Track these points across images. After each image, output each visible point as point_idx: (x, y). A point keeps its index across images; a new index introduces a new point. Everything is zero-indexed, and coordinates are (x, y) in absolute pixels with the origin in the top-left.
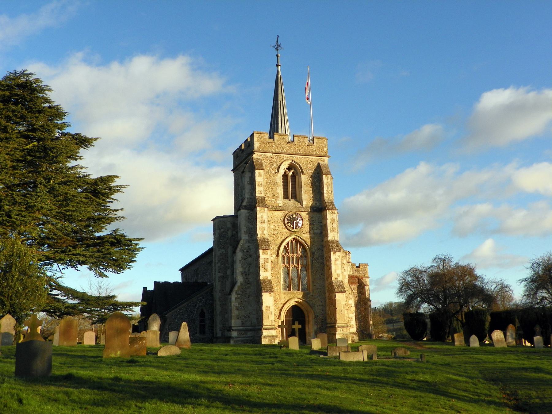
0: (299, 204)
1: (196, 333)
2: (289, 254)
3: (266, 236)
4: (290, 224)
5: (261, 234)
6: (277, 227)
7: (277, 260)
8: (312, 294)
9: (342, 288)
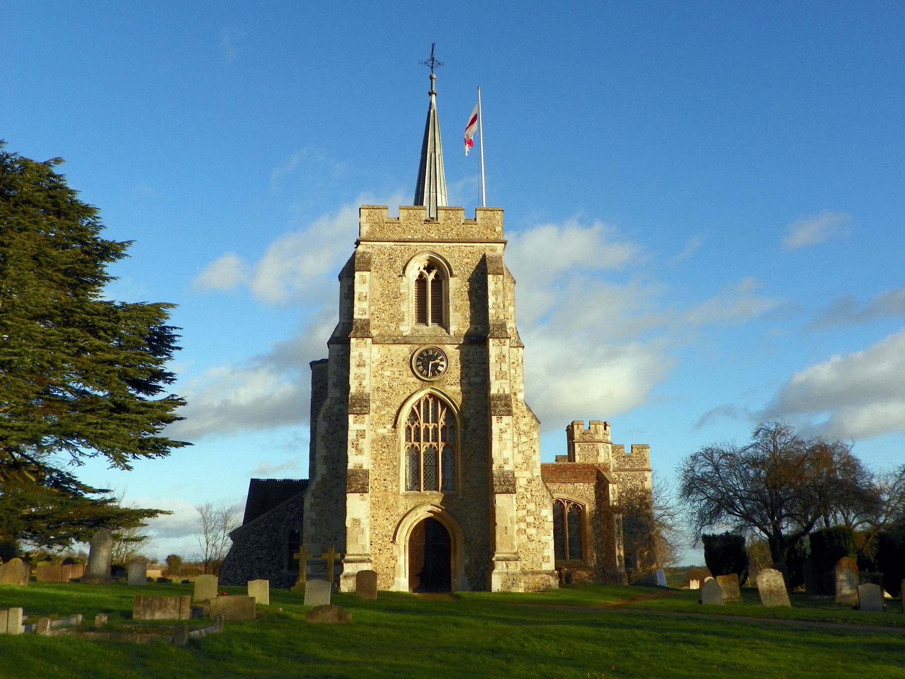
0: (444, 330)
1: (282, 567)
2: (419, 423)
3: (367, 390)
4: (421, 367)
5: (356, 387)
6: (397, 375)
7: (394, 434)
8: (461, 497)
9: (510, 485)
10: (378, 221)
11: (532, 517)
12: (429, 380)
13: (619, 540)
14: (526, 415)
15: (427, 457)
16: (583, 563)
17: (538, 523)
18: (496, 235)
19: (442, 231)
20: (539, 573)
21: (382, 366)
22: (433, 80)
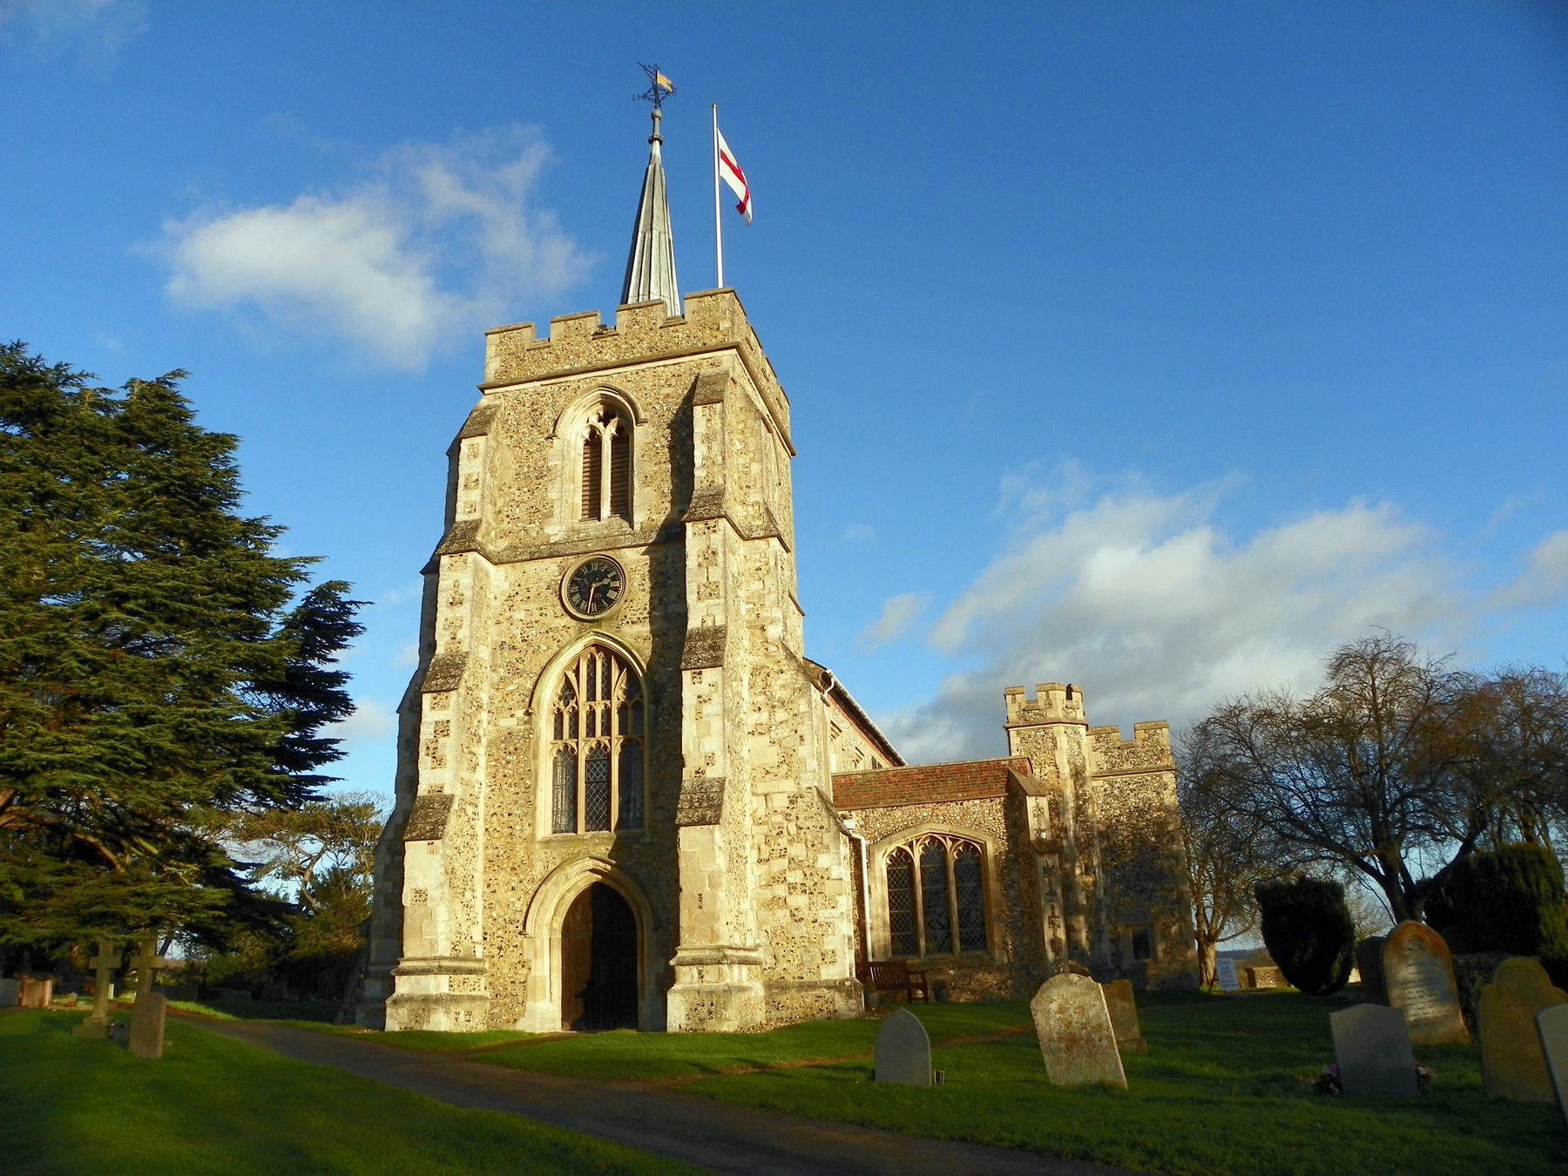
0: (625, 524)
4: (578, 596)
5: (447, 643)
6: (536, 616)
8: (648, 840)
9: (710, 807)
10: (514, 349)
11: (799, 873)
12: (592, 618)
13: (1053, 908)
14: (784, 668)
15: (592, 766)
16: (986, 957)
17: (812, 884)
18: (720, 337)
19: (624, 346)
20: (813, 986)
21: (510, 603)
22: (657, 120)
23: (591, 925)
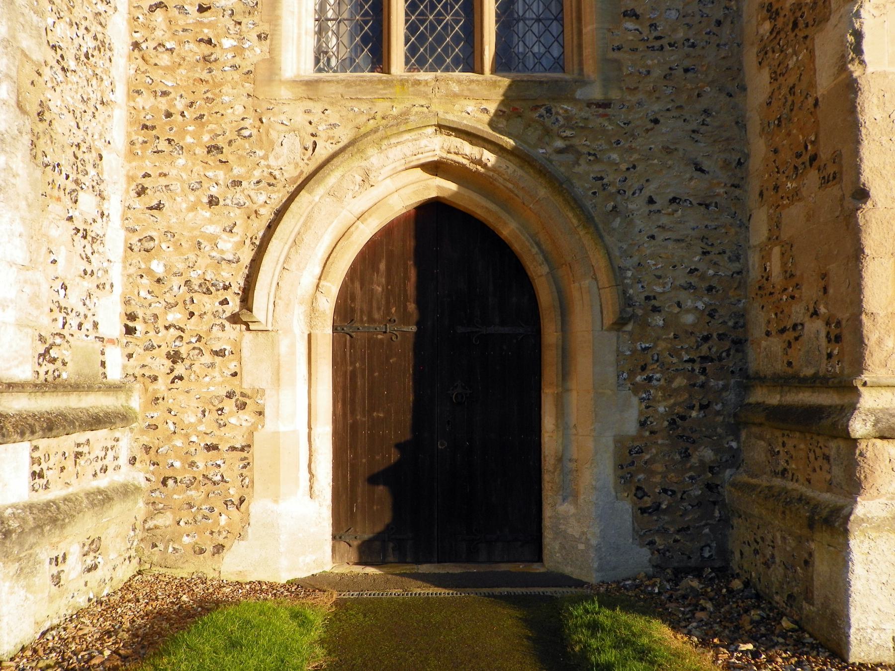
8: (596, 93)
23: (412, 307)
